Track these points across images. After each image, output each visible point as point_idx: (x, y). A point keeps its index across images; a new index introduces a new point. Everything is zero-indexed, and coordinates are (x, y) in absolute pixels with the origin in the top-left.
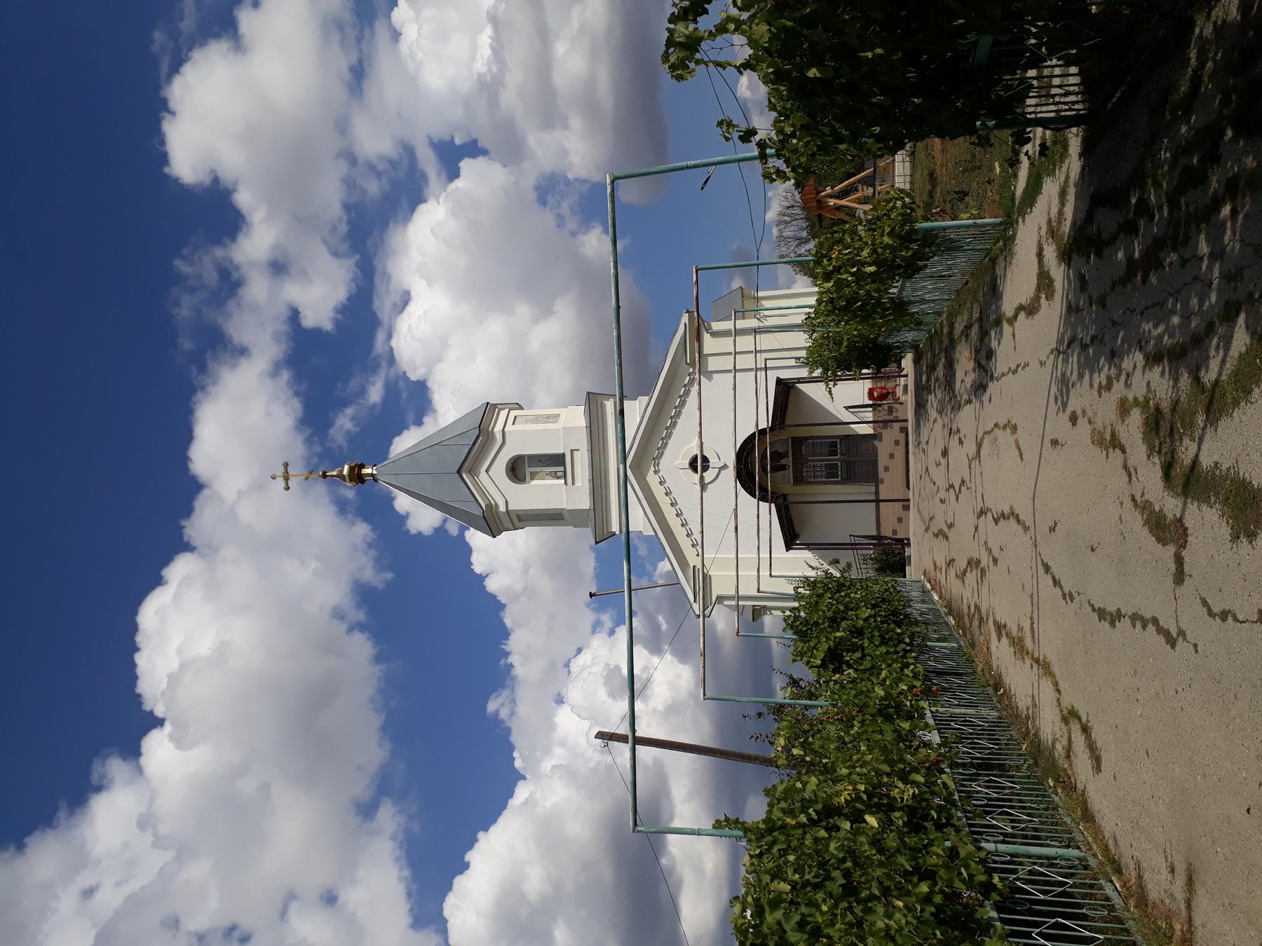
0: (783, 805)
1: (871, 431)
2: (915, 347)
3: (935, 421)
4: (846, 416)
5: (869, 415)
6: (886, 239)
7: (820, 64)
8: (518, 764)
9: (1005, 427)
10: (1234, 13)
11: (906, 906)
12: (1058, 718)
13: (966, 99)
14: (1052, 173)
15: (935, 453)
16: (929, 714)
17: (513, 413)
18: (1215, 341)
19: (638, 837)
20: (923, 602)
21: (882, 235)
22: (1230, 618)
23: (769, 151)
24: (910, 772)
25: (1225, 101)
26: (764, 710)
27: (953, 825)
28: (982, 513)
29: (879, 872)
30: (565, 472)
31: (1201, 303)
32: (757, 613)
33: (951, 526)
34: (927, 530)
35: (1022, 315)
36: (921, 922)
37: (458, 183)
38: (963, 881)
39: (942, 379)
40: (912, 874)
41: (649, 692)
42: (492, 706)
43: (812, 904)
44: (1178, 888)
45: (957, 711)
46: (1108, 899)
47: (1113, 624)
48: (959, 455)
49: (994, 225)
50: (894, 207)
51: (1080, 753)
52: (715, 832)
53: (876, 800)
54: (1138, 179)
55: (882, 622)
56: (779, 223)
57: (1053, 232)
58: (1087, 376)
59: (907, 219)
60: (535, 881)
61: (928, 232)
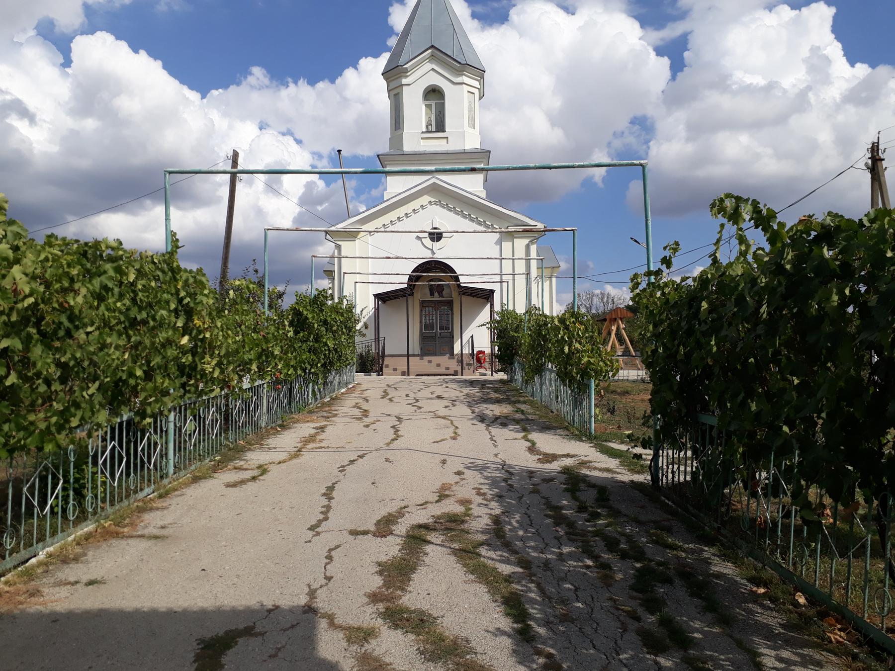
0: (191, 280)
1: (455, 352)
2: (511, 380)
3: (461, 392)
4: (466, 336)
5: (466, 351)
6: (586, 359)
7: (710, 311)
8: (215, 93)
9: (456, 433)
10: (714, 569)
11: (125, 360)
12: (261, 462)
13: (676, 411)
14: (622, 464)
15: (439, 391)
16: (261, 382)
17: (476, 91)
18: (506, 555)
19: (163, 183)
20: (340, 383)
21: (589, 357)
22: (327, 561)
23: (653, 277)
24: (220, 368)
25: (660, 564)
26: (260, 274)
27: (184, 395)
28: (399, 419)
29: (147, 342)
30: (431, 132)
31: (530, 547)
32: (329, 274)
33: (391, 400)
34: (388, 386)
35: (529, 444)
36: (115, 370)
37: (653, 54)
38: (146, 398)
39: (489, 396)
40: (148, 365)
41: (271, 195)
42: (257, 71)
43: (121, 297)
44: (151, 530)
45: (265, 401)
46: (142, 490)
47: (324, 495)
48: (439, 406)
49: (590, 429)
50: (606, 365)
51: (238, 475)
52: (169, 232)
53: (199, 344)
54: (615, 513)
55: (325, 355)
56: (603, 294)
57: (582, 464)
58: (487, 481)
59: (598, 373)
60: (127, 105)
61: (588, 386)
